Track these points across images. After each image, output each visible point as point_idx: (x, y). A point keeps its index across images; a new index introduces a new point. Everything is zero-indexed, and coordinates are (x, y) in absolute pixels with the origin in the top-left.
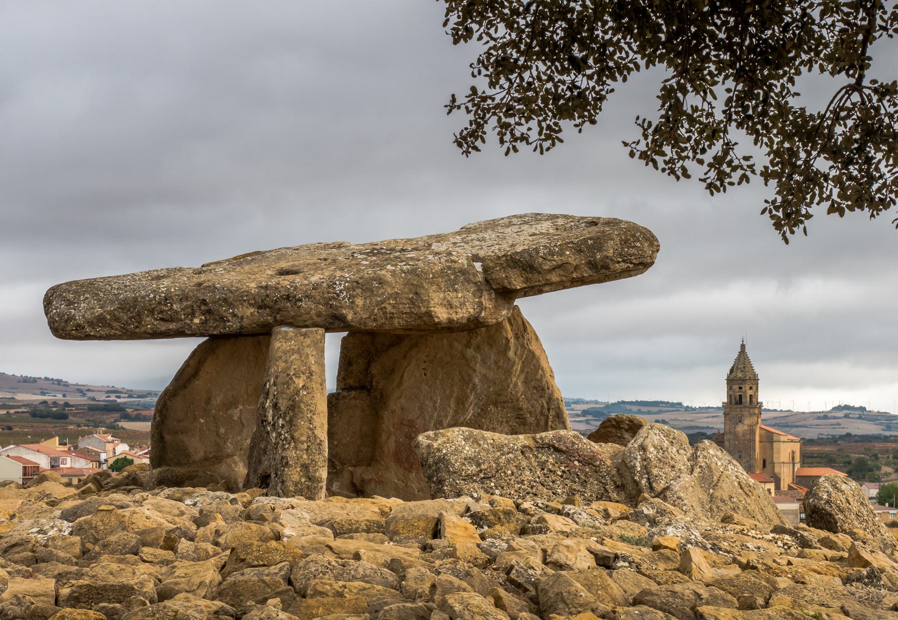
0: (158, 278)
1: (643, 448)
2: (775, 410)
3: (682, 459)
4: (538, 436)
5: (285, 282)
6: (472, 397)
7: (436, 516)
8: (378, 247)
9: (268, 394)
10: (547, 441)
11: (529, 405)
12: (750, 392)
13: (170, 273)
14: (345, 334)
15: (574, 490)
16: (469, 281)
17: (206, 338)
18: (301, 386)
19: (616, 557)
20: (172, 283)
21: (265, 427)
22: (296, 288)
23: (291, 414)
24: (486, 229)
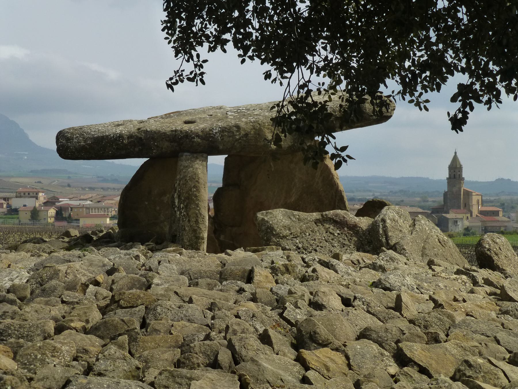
0: (118, 125)
1: (384, 221)
4: (324, 213)
5: (186, 127)
6: (294, 190)
7: (251, 268)
8: (241, 109)
9: (176, 190)
10: (329, 216)
12: (459, 173)
13: (123, 124)
14: (227, 156)
15: (344, 244)
17: (148, 159)
18: (192, 186)
20: (124, 128)
21: (174, 208)
22: (191, 131)
23: (187, 201)
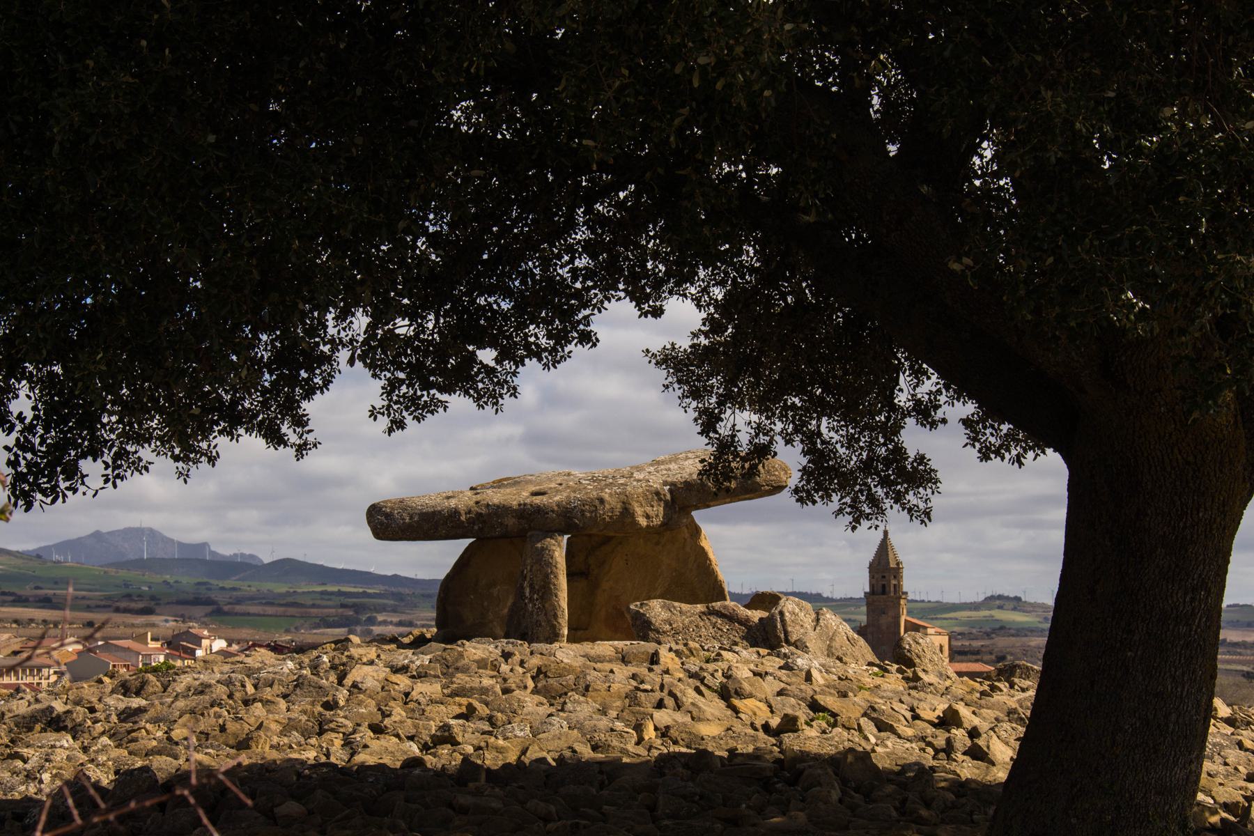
0: (448, 498)
1: (781, 613)
2: (923, 601)
3: (808, 621)
5: (537, 500)
11: (699, 583)
12: (894, 582)
16: (660, 500)
19: (766, 673)
24: (670, 462)
